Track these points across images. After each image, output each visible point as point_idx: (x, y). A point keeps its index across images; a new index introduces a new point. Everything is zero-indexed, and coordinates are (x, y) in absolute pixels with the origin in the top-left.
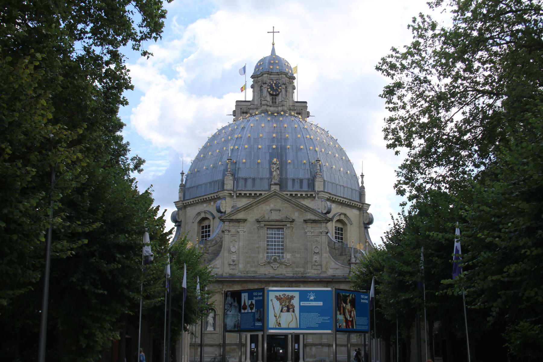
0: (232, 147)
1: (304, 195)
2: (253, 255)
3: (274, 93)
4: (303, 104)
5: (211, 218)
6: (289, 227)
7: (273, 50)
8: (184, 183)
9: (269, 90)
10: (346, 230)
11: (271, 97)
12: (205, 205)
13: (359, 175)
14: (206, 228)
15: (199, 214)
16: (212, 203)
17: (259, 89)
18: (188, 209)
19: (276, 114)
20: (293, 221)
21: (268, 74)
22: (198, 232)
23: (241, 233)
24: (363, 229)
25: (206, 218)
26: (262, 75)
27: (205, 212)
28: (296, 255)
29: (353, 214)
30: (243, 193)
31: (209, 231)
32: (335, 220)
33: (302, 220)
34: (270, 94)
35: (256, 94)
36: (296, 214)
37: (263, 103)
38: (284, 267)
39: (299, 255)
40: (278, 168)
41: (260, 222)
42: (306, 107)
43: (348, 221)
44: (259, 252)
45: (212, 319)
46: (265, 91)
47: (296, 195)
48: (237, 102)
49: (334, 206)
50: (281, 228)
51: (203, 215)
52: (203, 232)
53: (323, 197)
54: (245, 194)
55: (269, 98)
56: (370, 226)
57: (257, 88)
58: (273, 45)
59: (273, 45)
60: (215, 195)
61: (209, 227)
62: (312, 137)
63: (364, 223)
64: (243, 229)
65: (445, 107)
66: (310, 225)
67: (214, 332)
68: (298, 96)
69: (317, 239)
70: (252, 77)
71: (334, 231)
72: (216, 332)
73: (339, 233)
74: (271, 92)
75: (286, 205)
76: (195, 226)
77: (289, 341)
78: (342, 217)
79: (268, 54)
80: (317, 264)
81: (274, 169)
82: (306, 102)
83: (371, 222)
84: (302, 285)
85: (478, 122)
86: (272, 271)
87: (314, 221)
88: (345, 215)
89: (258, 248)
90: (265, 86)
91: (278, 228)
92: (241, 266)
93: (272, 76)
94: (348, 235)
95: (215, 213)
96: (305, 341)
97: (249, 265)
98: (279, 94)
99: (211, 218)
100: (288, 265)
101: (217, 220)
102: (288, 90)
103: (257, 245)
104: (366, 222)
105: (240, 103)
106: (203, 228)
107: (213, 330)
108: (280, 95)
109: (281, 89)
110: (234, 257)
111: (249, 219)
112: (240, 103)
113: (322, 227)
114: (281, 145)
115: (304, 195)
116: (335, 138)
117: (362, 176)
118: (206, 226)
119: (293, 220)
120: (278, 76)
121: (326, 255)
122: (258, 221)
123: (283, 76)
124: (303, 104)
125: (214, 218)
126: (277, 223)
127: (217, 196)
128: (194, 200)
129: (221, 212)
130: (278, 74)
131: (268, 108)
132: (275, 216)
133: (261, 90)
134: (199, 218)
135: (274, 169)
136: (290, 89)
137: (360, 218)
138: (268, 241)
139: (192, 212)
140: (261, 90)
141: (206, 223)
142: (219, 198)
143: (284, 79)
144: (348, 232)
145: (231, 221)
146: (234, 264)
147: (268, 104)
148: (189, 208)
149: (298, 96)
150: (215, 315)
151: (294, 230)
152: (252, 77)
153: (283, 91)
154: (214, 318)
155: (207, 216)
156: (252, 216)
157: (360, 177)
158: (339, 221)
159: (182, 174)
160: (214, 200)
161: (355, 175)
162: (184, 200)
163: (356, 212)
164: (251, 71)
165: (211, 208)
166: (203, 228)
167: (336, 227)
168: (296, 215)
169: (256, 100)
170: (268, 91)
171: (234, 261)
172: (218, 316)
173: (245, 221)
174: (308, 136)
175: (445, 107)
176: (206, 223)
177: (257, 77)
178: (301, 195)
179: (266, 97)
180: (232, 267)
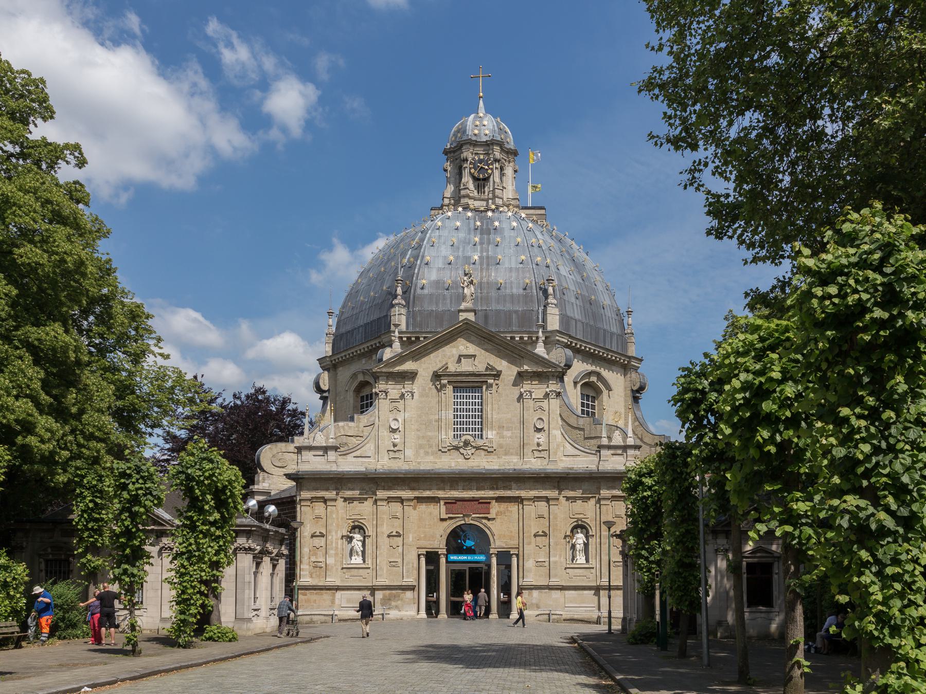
1: (526, 339)
2: (429, 434)
3: (481, 176)
11: (476, 184)
14: (367, 400)
15: (354, 376)
27: (364, 373)
37: (463, 192)
39: (508, 434)
41: (440, 376)
43: (604, 385)
44: (439, 429)
45: (360, 544)
50: (478, 387)
51: (361, 378)
53: (558, 340)
67: (363, 566)
69: (541, 404)
72: (367, 566)
73: (588, 407)
74: (476, 175)
77: (492, 581)
78: (594, 379)
80: (540, 448)
81: (466, 284)
84: (514, 485)
85: (837, 122)
86: (461, 460)
88: (598, 375)
91: (473, 387)
92: (409, 453)
96: (521, 580)
97: (422, 451)
98: (489, 177)
100: (489, 450)
102: (505, 172)
104: (635, 388)
106: (362, 398)
107: (362, 562)
109: (492, 169)
114: (488, 257)
115: (526, 339)
118: (367, 396)
119: (498, 371)
121: (557, 433)
127: (380, 343)
128: (346, 353)
132: (466, 366)
134: (355, 384)
135: (466, 284)
138: (456, 410)
147: (471, 195)
148: (341, 369)
151: (500, 390)
153: (497, 173)
156: (425, 367)
166: (362, 399)
168: (502, 365)
170: (470, 172)
171: (395, 445)
172: (370, 539)
176: (365, 392)
178: (521, 338)
179: (467, 182)
180: (392, 455)
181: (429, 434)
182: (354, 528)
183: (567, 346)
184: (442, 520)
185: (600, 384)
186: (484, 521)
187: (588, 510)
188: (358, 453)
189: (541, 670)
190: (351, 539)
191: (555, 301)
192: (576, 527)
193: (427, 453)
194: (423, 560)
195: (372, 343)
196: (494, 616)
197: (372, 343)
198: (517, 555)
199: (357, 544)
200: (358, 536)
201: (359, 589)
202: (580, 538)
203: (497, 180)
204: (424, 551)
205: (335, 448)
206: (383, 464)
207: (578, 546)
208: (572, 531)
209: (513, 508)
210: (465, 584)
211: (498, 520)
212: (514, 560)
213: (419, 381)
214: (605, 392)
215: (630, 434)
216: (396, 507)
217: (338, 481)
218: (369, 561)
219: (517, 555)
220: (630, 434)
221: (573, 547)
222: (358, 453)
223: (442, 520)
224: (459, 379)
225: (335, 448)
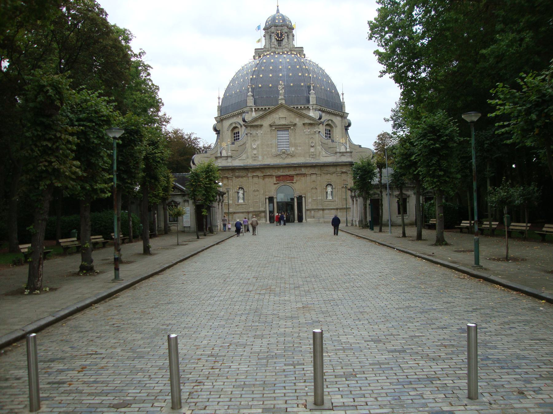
0: (251, 77)
2: (268, 149)
4: (301, 49)
5: (239, 126)
6: (292, 129)
7: (278, 11)
8: (220, 104)
9: (276, 37)
10: (333, 131)
12: (235, 118)
13: (340, 93)
15: (231, 124)
16: (240, 117)
17: (269, 37)
18: (224, 122)
19: (281, 53)
20: (295, 125)
21: (275, 26)
22: (231, 137)
23: (259, 135)
24: (344, 130)
25: (236, 127)
26: (271, 28)
28: (298, 148)
29: (337, 120)
30: (260, 108)
31: (239, 136)
32: (325, 124)
33: (302, 124)
34: (277, 40)
35: (267, 40)
36: (297, 120)
38: (290, 157)
40: (283, 88)
42: (303, 51)
46: (273, 38)
47: (297, 107)
48: (255, 49)
49: (323, 114)
51: (234, 125)
52: (234, 137)
54: (262, 109)
55: (276, 43)
56: (349, 128)
57: (268, 37)
58: (278, 6)
59: (278, 6)
60: (241, 110)
61: (239, 133)
62: (307, 67)
63: (345, 127)
64: (260, 132)
65: (411, 20)
66: (307, 127)
68: (297, 43)
70: (264, 29)
71: (325, 132)
74: (278, 39)
75: (290, 113)
76: (229, 133)
78: (330, 122)
79: (274, 12)
82: (302, 48)
83: (349, 125)
87: (311, 124)
88: (332, 121)
89: (271, 144)
90: (273, 35)
92: (260, 158)
93: (278, 28)
94: (334, 135)
95: (242, 123)
96: (306, 207)
98: (283, 40)
99: (239, 126)
101: (244, 128)
103: (271, 143)
105: (257, 51)
108: (284, 40)
110: (255, 152)
111: (264, 124)
112: (257, 51)
113: (316, 129)
116: (323, 69)
117: (343, 94)
120: (281, 28)
122: (271, 126)
123: (285, 27)
124: (301, 49)
125: (241, 126)
126: (284, 127)
129: (246, 122)
130: (282, 26)
131: (276, 50)
132: (283, 122)
133: (270, 38)
136: (291, 37)
137: (342, 122)
139: (227, 124)
140: (270, 38)
141: (236, 131)
142: (244, 112)
143: (285, 30)
144: (334, 132)
145: (252, 126)
146: (255, 157)
149: (297, 43)
150: (244, 192)
152: (264, 29)
153: (286, 37)
154: (243, 194)
155: (237, 125)
156: (266, 123)
157: (341, 95)
158: (327, 125)
159: (219, 98)
160: (241, 114)
161: (338, 94)
162: (221, 116)
163: (339, 119)
164: (263, 26)
165: (239, 120)
167: (326, 129)
168: (297, 120)
169: (267, 45)
173: (261, 126)
174: (304, 67)
175: (411, 20)
176: (236, 131)
177: (268, 29)
178: (301, 107)
181: (268, 149)
182: (239, 188)
183: (320, 110)
184: (275, 184)
185: (332, 124)
186: (291, 184)
187: (333, 179)
188: (240, 159)
189: (382, 205)
190: (238, 193)
191: (314, 92)
192: (327, 185)
193: (267, 157)
194: (267, 200)
195: (239, 111)
196: (296, 221)
197: (239, 111)
198: (305, 197)
199: (241, 195)
200: (241, 192)
201: (243, 213)
202: (329, 189)
203: (286, 41)
204: (267, 197)
205: (231, 157)
206: (250, 162)
207: (328, 193)
208: (326, 187)
209: (303, 178)
210: (155, 225)
211: (297, 183)
212: (303, 199)
213: (264, 128)
214: (334, 128)
215: (348, 147)
216: (256, 180)
217: (233, 169)
218: (246, 201)
219: (305, 197)
220: (348, 147)
221: (327, 193)
222: (240, 159)
223: (275, 184)
224: (281, 127)
225: (231, 157)
